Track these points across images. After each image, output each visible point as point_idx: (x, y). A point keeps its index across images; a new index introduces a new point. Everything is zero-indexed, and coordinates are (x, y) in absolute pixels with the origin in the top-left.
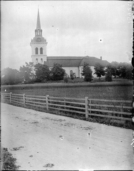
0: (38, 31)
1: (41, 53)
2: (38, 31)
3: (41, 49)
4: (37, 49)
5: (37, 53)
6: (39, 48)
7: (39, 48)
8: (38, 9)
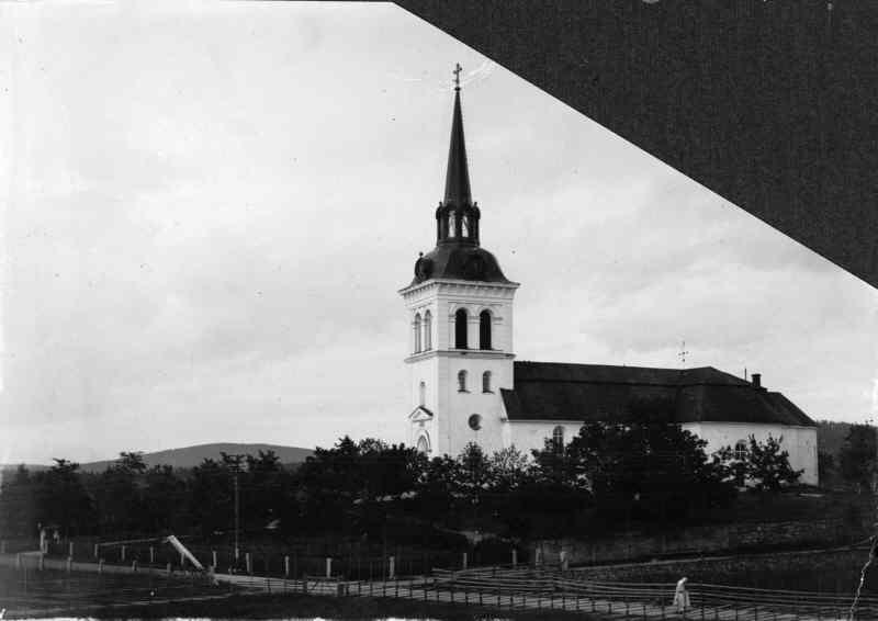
0: (459, 206)
1: (486, 342)
2: (459, 206)
3: (486, 318)
4: (461, 318)
5: (461, 341)
6: (474, 312)
7: (474, 312)
8: (458, 89)
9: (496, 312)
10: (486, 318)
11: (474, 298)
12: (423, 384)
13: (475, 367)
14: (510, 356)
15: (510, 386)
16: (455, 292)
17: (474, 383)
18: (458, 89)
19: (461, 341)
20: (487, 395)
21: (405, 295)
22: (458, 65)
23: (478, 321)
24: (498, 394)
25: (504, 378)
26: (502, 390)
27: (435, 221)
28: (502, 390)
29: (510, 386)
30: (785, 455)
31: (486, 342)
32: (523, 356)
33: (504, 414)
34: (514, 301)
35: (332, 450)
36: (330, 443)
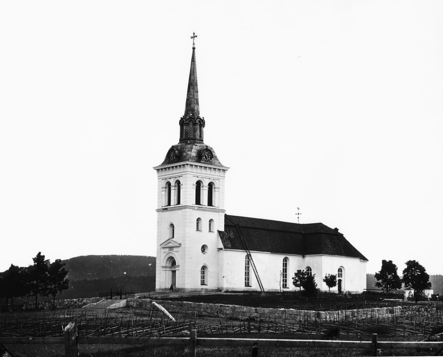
0: (191, 123)
1: (210, 203)
2: (191, 123)
5: (198, 201)
6: (205, 183)
7: (205, 183)
8: (194, 49)
9: (217, 184)
10: (211, 185)
11: (206, 175)
12: (172, 225)
13: (206, 216)
14: (223, 211)
15: (222, 229)
16: (199, 170)
17: (204, 225)
18: (194, 49)
19: (198, 201)
20: (211, 233)
21: (158, 170)
22: (194, 34)
23: (207, 189)
24: (216, 233)
25: (220, 225)
26: (219, 232)
27: (179, 127)
28: (219, 232)
29: (222, 229)
30: (413, 266)
31: (210, 203)
32: (230, 213)
33: (221, 246)
34: (225, 178)
35: (364, 292)
36: (26, 261)
